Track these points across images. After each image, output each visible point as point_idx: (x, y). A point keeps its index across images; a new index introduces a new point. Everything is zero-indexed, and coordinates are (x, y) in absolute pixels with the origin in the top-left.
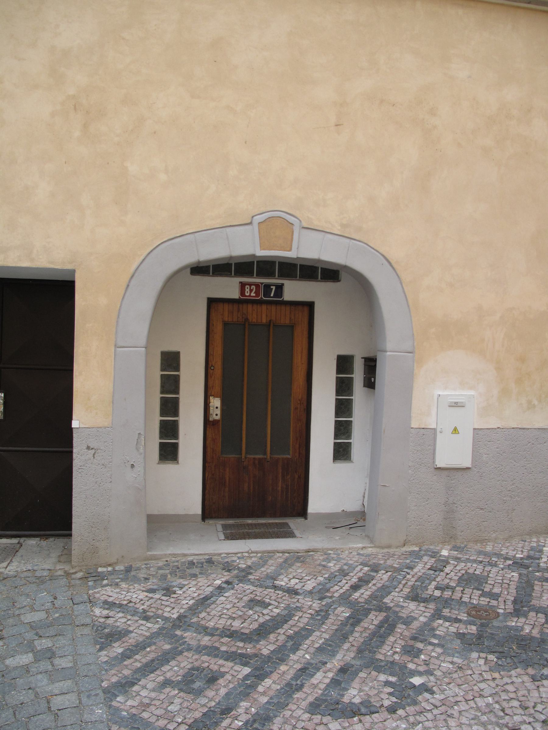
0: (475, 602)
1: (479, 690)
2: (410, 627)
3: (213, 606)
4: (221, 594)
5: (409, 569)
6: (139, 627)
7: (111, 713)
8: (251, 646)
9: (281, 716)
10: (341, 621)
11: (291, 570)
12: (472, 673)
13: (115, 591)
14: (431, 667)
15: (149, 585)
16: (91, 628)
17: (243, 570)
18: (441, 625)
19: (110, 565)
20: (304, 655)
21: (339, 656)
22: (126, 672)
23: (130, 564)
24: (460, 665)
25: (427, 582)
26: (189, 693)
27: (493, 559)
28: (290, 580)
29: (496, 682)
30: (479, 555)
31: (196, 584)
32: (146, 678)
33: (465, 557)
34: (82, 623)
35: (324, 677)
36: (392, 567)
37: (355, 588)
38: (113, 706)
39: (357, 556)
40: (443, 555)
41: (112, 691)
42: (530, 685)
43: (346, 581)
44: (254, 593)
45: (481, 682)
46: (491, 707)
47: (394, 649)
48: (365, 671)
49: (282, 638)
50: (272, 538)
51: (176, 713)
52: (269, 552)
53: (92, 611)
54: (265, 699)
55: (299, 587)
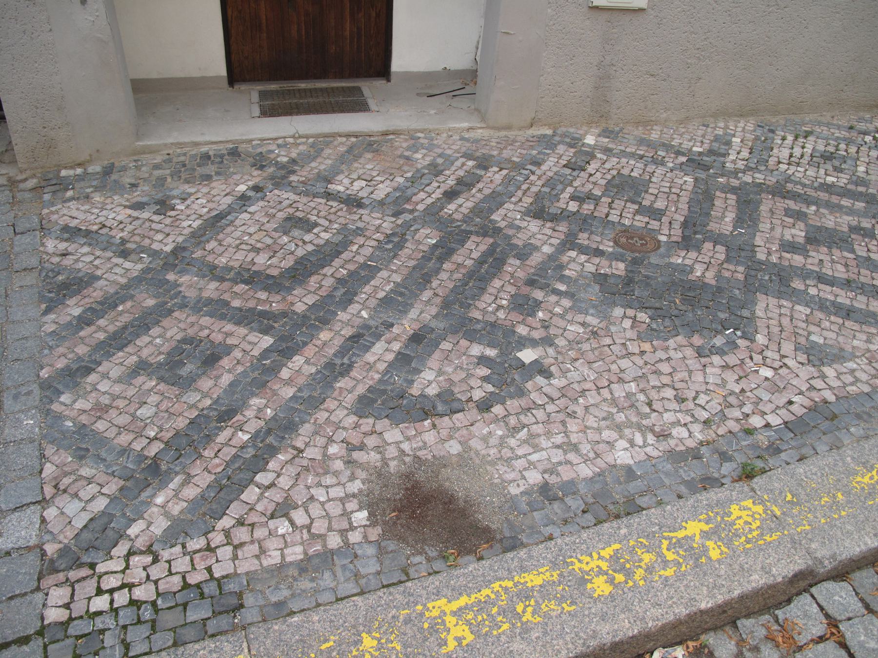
0: (627, 222)
1: (618, 371)
2: (528, 262)
3: (229, 229)
4: (244, 208)
5: (535, 166)
6: (111, 268)
7: (48, 423)
8: (278, 298)
9: (312, 421)
10: (424, 251)
11: (356, 165)
12: (612, 342)
13: (83, 208)
14: (552, 331)
15: (137, 196)
16: (37, 274)
17: (282, 167)
18: (574, 261)
19: (80, 165)
20: (360, 311)
21: (413, 314)
22: (82, 350)
23: (112, 161)
24: (595, 329)
25: (560, 187)
26: (173, 385)
27: (659, 153)
28: (352, 182)
29: (647, 357)
30: (640, 145)
31: (208, 193)
32: (111, 359)
33: (620, 148)
34: (24, 266)
35: (387, 350)
36: (509, 161)
37: (451, 195)
38: (53, 411)
39: (459, 143)
40: (588, 144)
41: (55, 384)
42: (693, 363)
43: (437, 184)
44: (294, 205)
45: (623, 357)
46: (633, 399)
47: (498, 302)
48: (451, 340)
49: (328, 282)
50: (334, 111)
51: (148, 421)
52: (326, 136)
53: (43, 245)
54: (289, 392)
55: (365, 195)
